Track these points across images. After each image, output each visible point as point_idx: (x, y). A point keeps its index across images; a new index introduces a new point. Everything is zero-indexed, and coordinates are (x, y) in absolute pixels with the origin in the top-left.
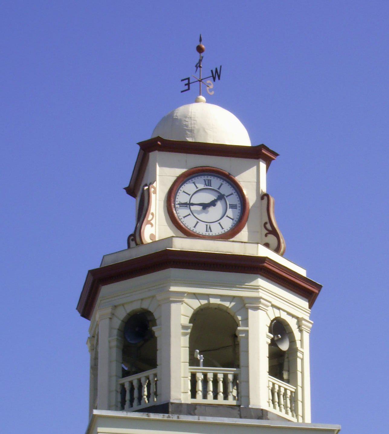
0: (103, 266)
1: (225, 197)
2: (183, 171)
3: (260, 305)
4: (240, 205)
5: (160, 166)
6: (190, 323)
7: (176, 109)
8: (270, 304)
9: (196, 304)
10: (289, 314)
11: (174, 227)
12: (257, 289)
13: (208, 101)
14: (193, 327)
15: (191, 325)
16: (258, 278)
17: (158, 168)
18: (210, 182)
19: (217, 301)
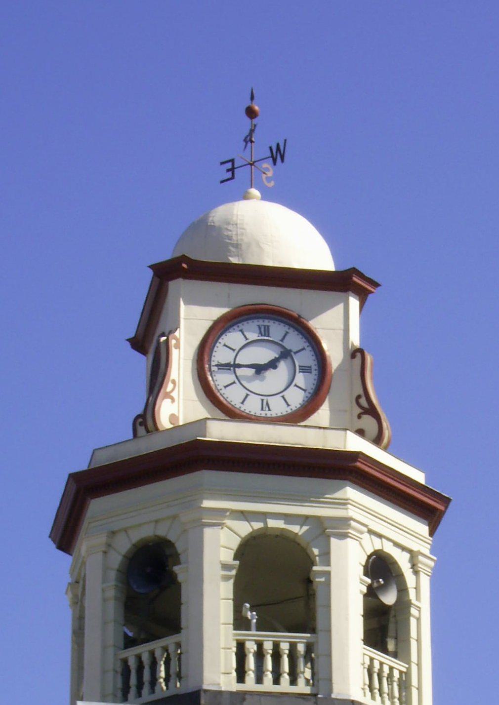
0: (92, 467)
1: (293, 354)
3: (350, 531)
4: (316, 368)
6: (235, 559)
9: (245, 528)
10: (396, 545)
14: (240, 566)
15: (237, 563)
16: (346, 486)
18: (268, 329)
19: (279, 524)
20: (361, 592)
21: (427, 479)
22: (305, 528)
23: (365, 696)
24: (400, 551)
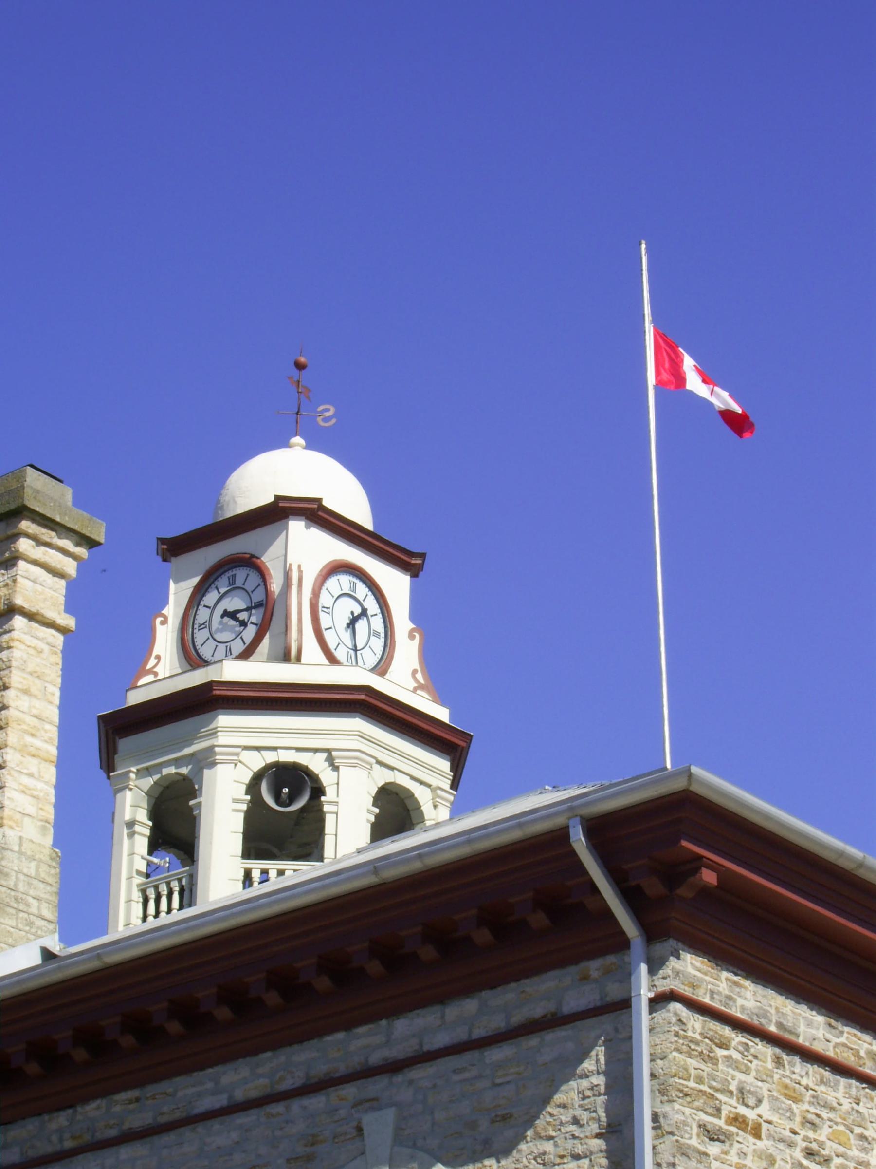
2: (195, 580)
3: (217, 757)
5: (176, 582)
6: (247, 794)
7: (224, 492)
8: (240, 749)
9: (149, 782)
10: (299, 750)
11: (184, 660)
12: (216, 733)
13: (309, 446)
14: (251, 801)
15: (248, 797)
16: (217, 716)
17: (172, 583)
19: (172, 770)
20: (368, 821)
21: (452, 716)
22: (190, 767)
23: (299, 566)
24: (311, 754)
